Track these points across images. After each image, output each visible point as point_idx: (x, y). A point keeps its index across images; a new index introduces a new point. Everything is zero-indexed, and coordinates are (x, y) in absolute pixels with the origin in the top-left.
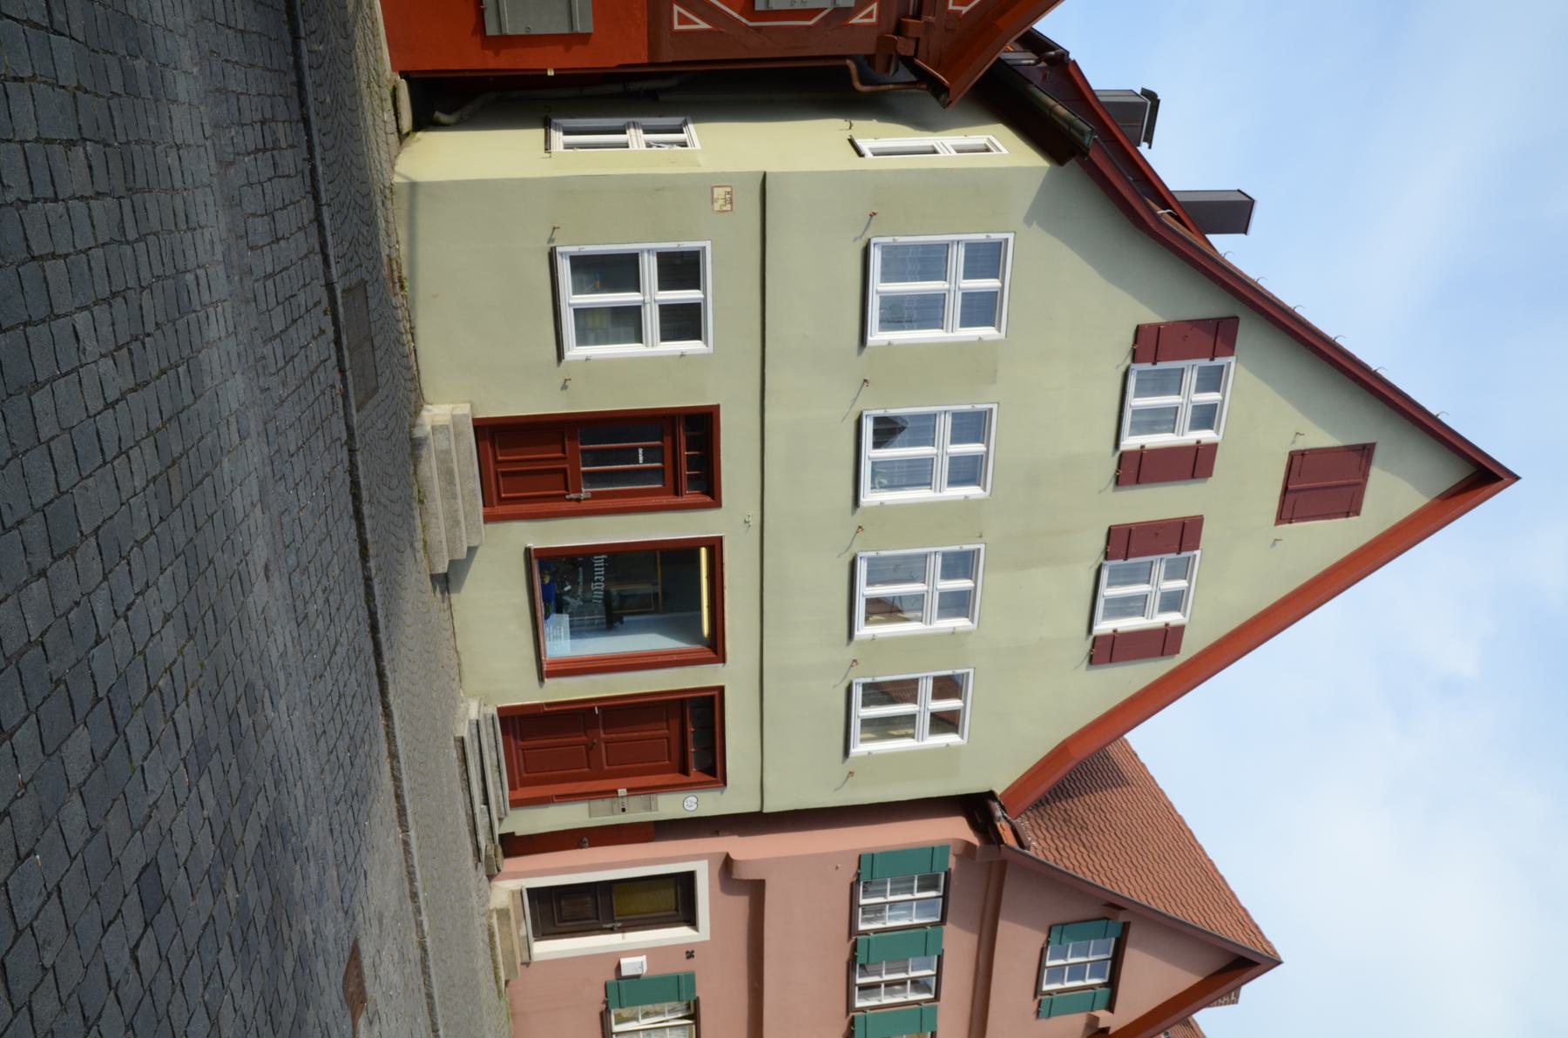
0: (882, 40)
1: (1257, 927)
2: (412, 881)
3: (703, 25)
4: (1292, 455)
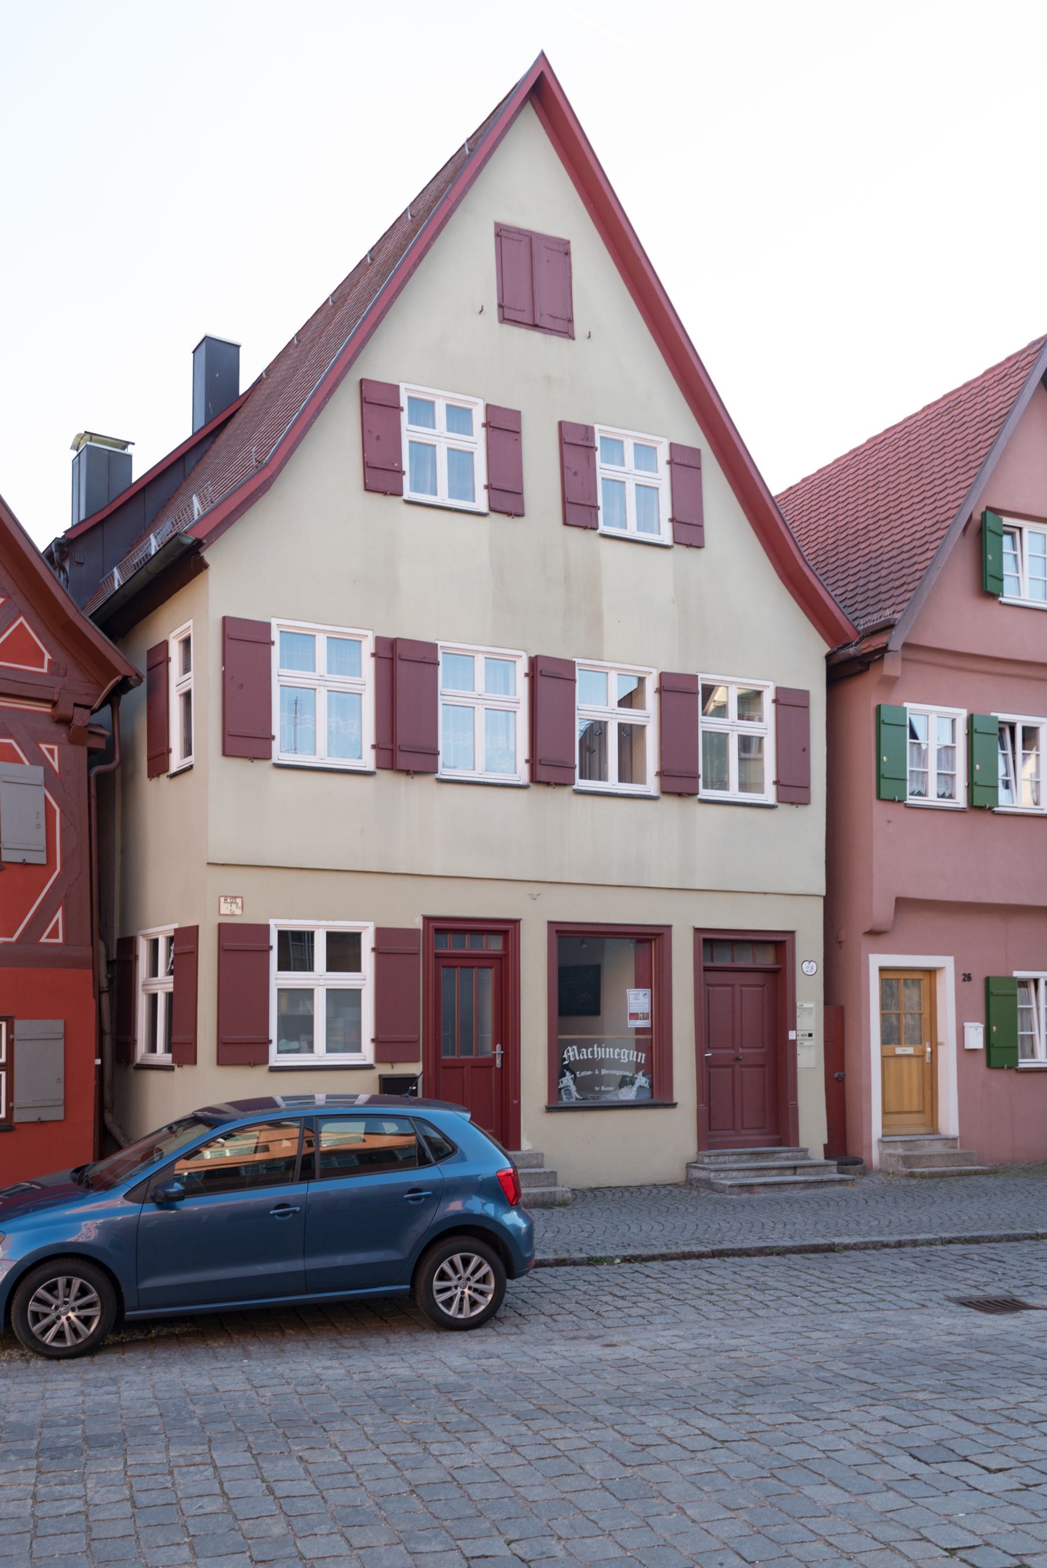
0: (73, 741)
1: (1009, 359)
2: (886, 1245)
3: (59, 914)
4: (504, 319)
